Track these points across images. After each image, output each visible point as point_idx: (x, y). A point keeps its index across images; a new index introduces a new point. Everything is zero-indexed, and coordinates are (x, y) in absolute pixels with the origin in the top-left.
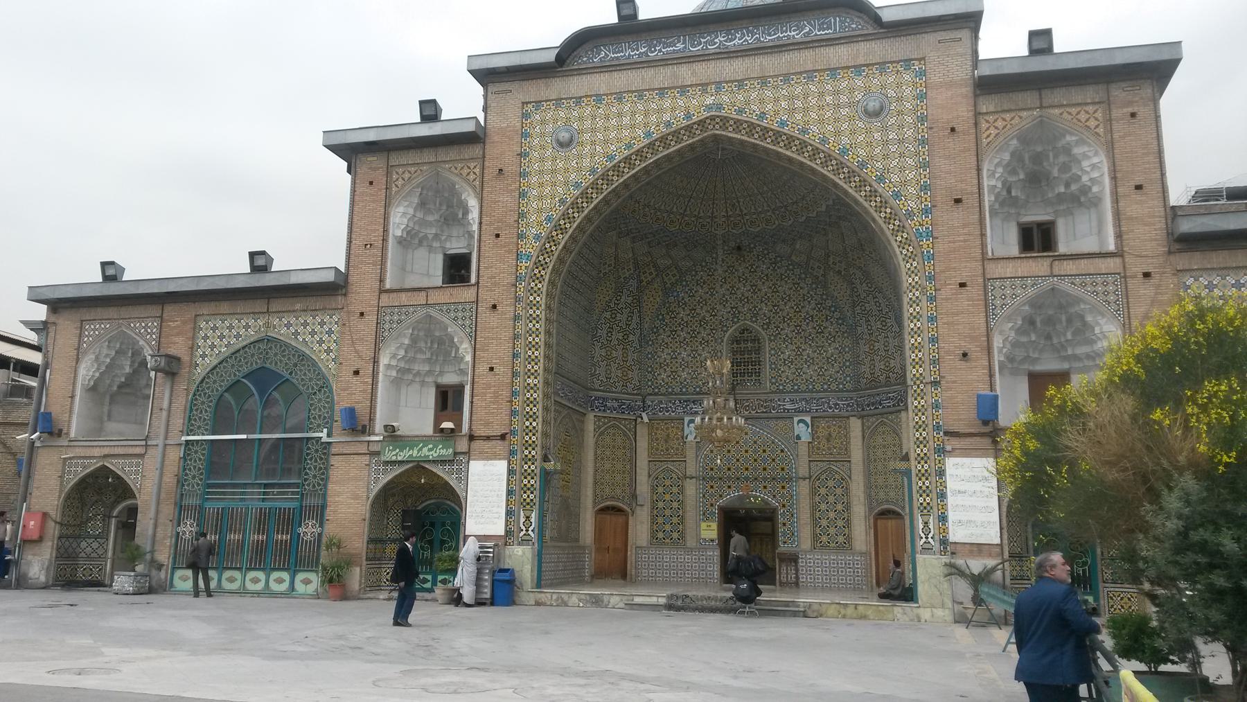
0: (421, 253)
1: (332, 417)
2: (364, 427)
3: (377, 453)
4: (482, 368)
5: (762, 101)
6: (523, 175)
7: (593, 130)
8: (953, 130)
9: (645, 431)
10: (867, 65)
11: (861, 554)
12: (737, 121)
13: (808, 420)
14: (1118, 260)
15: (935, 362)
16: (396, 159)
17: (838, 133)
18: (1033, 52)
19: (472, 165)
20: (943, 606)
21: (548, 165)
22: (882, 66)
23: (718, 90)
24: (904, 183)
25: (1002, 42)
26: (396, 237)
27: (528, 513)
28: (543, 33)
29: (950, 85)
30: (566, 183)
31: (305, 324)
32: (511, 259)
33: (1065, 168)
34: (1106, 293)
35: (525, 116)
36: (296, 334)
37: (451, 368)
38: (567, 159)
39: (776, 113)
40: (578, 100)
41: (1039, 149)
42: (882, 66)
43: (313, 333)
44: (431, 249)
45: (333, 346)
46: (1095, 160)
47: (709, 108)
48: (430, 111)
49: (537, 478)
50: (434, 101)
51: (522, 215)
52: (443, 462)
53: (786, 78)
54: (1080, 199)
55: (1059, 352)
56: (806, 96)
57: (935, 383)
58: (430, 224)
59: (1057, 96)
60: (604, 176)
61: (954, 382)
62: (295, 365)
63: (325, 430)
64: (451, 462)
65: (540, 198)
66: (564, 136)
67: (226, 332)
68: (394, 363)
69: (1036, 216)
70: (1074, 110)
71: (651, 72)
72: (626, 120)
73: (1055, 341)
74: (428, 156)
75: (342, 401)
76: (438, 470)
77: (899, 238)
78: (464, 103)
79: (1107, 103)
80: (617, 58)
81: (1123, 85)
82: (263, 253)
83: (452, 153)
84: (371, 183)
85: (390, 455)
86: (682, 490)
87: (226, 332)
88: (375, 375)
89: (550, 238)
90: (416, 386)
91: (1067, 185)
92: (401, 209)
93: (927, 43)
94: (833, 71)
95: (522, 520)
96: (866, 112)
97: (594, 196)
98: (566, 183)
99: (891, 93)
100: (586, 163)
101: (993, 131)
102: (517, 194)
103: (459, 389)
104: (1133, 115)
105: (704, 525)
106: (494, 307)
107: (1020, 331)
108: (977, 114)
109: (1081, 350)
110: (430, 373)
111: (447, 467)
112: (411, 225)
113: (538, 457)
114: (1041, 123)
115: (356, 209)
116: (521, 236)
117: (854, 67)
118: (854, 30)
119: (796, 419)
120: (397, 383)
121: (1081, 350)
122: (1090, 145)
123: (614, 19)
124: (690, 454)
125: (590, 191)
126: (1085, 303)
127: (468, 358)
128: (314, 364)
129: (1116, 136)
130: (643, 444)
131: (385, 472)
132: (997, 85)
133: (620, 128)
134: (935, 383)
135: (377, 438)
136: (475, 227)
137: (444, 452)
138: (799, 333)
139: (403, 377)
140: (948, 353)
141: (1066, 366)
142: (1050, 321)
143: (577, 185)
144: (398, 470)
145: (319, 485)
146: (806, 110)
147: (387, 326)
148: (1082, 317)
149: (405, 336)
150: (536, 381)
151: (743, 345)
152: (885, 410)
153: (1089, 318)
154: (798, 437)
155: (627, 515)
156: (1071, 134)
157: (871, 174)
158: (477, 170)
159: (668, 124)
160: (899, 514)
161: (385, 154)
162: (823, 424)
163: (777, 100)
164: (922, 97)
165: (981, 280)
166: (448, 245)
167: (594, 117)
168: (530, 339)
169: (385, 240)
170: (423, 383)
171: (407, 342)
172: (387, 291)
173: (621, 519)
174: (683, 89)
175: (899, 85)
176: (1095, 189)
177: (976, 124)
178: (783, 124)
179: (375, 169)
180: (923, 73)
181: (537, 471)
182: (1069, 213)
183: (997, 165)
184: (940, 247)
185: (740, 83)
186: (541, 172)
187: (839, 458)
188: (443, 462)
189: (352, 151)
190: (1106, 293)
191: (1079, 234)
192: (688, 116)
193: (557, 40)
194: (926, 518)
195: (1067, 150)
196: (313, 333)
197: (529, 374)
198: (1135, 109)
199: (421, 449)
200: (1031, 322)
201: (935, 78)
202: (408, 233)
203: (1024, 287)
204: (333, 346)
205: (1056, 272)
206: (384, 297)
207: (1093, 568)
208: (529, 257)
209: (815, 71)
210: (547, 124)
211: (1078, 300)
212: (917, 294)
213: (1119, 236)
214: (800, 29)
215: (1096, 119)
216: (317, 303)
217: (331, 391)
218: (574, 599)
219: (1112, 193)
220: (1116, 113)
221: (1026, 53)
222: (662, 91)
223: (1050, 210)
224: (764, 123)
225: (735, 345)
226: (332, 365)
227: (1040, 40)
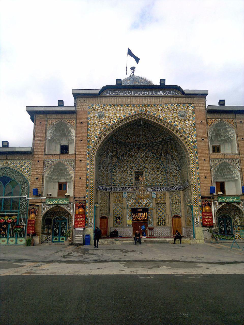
0: (54, 144)
1: (29, 192)
2: (40, 194)
3: (45, 202)
4: (77, 178)
5: (154, 110)
6: (89, 124)
7: (109, 113)
8: (201, 122)
9: (112, 195)
10: (181, 104)
11: (169, 227)
12: (148, 115)
13: (155, 193)
14: (239, 156)
15: (199, 179)
16: (49, 116)
17: (174, 120)
18: (220, 105)
19: (73, 120)
20: (202, 239)
21: (96, 122)
22: (184, 104)
23: (143, 106)
24: (190, 134)
25: (211, 101)
26: (48, 139)
27: (197, 218)
28: (96, 85)
29: (200, 111)
30: (101, 127)
31: (19, 164)
32: (86, 147)
33: (224, 133)
34: (236, 163)
35: (89, 108)
36: (16, 166)
37: (63, 178)
38: (101, 121)
39: (158, 113)
40: (104, 105)
41: (219, 128)
42: (184, 104)
43: (22, 166)
44: (56, 143)
45: (29, 170)
46: (232, 132)
47: (141, 110)
48: (61, 103)
49: (93, 209)
50: (63, 101)
51: (88, 135)
52: (66, 205)
53: (161, 105)
54: (228, 140)
55: (223, 177)
56: (166, 110)
57: (199, 184)
58: (57, 136)
59: (225, 116)
60: (112, 126)
61: (203, 184)
62: (16, 176)
63: (27, 195)
64: (68, 205)
65: (94, 131)
66: (101, 114)
67: (23, 165)
68: (48, 176)
69: (216, 144)
70: (228, 120)
71: (125, 99)
72: (118, 112)
73: (222, 174)
74: (59, 116)
75: (32, 187)
76: (64, 207)
77: (189, 148)
78: (70, 102)
79: (235, 119)
80: (115, 95)
81: (239, 114)
82: (7, 141)
83: (67, 116)
84: (41, 123)
85: (49, 203)
86: (122, 211)
87: (23, 165)
88: (43, 179)
89: (96, 142)
90: (52, 183)
91: (224, 137)
92: (50, 131)
93: (195, 99)
94: (172, 104)
95: (90, 221)
96: (181, 116)
97: (109, 131)
98: (101, 127)
99: (186, 111)
100: (107, 122)
101: (210, 123)
102: (87, 129)
103: (66, 184)
104: (241, 122)
105: (128, 221)
106: (81, 161)
107: (216, 172)
108: (207, 119)
109: (228, 177)
110: (57, 179)
111: (67, 206)
112: (52, 135)
113: (94, 203)
114: (221, 122)
115: (36, 130)
116: (88, 141)
117: (178, 104)
118: (177, 95)
119: (152, 193)
120: (48, 182)
121: (228, 177)
122: (231, 128)
123: (159, 84)
124: (125, 202)
125: (108, 130)
126: (232, 165)
127: (73, 175)
128: (22, 176)
129: (237, 126)
130: (112, 199)
131: (47, 208)
132: (211, 111)
133: (116, 113)
134: (199, 184)
135: (44, 198)
136: (74, 138)
137: (66, 202)
138: (153, 170)
139: (50, 180)
140: (202, 176)
141: (224, 180)
142: (222, 169)
143: (104, 128)
144: (51, 207)
145: (25, 212)
146: (166, 114)
147: (47, 165)
148: (230, 169)
149: (52, 168)
150: (93, 182)
151: (138, 173)
152: (175, 191)
153: (232, 169)
154: (153, 197)
155: (107, 219)
156: (227, 125)
157: (182, 131)
158: (74, 122)
159: (130, 114)
160: (179, 217)
161: (45, 115)
162: (159, 194)
163: (158, 110)
164: (194, 113)
165: (209, 159)
166: (61, 142)
167: (109, 110)
168: (91, 170)
169: (45, 140)
170: (55, 182)
171: (52, 170)
172: (47, 155)
173: (106, 220)
174: (134, 105)
175: (188, 110)
176: (232, 139)
177: (206, 121)
178: (160, 116)
179: (42, 119)
180: (194, 107)
181: (93, 207)
182: (223, 144)
183: (211, 131)
184: (199, 150)
185: (149, 105)
186: (94, 124)
187: (120, 203)
188: (66, 205)
189: (35, 114)
190: (236, 163)
191: (226, 149)
192: (135, 112)
193: (99, 88)
194: (91, 219)
195: (225, 129)
196: (22, 166)
197: (91, 180)
198: (241, 121)
199: (59, 201)
200: (218, 169)
201: (197, 108)
202: (51, 138)
203: (218, 161)
204: (29, 170)
205: (225, 158)
206: (46, 156)
207: (232, 229)
208: (91, 147)
209: (168, 104)
210: (95, 110)
211: (230, 165)
212: (194, 162)
213: (239, 150)
214: (163, 93)
215: (74, 122)
216: (24, 157)
217: (28, 184)
218: (106, 242)
219: (237, 140)
220: (237, 121)
221: (218, 105)
222: (128, 105)
223: (219, 143)
224: (155, 116)
225: (136, 173)
226: (28, 176)
227: (222, 102)
